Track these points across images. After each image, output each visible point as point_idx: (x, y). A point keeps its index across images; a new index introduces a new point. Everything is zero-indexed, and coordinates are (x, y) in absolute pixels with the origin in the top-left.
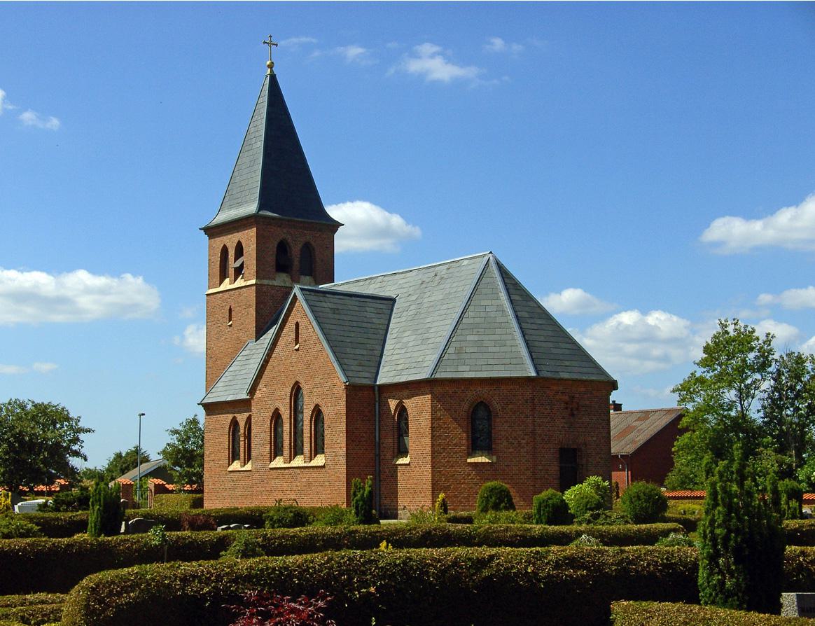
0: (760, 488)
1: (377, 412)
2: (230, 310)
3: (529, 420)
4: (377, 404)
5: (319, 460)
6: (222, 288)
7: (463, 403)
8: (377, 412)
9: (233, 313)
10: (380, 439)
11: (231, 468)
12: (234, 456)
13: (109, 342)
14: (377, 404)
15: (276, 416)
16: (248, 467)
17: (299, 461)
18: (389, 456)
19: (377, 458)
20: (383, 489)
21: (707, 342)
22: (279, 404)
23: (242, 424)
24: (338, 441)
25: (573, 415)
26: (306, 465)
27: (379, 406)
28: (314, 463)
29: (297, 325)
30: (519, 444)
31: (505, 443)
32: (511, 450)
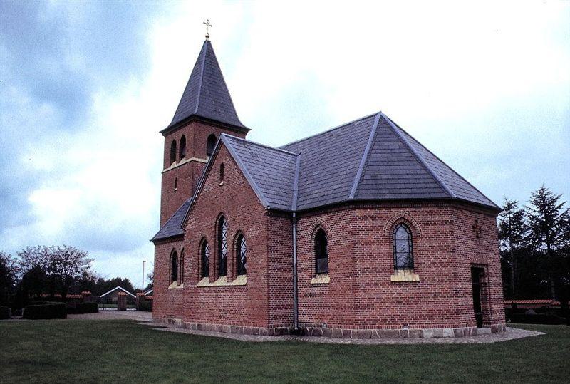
0: (553, 285)
1: (294, 237)
2: (176, 180)
3: (449, 241)
4: (294, 229)
5: (241, 280)
6: (171, 167)
7: (384, 224)
8: (294, 237)
9: (178, 183)
10: (297, 261)
11: (170, 287)
12: (174, 278)
13: (97, 200)
14: (294, 229)
15: (204, 242)
16: (182, 286)
17: (222, 281)
18: (306, 276)
19: (295, 278)
20: (300, 307)
21: (109, 274)
22: (205, 233)
23: (179, 254)
24: (260, 262)
25: (478, 237)
26: (228, 284)
27: (296, 231)
28: (235, 283)
29: (222, 165)
30: (441, 262)
31: (427, 263)
32: (434, 269)
